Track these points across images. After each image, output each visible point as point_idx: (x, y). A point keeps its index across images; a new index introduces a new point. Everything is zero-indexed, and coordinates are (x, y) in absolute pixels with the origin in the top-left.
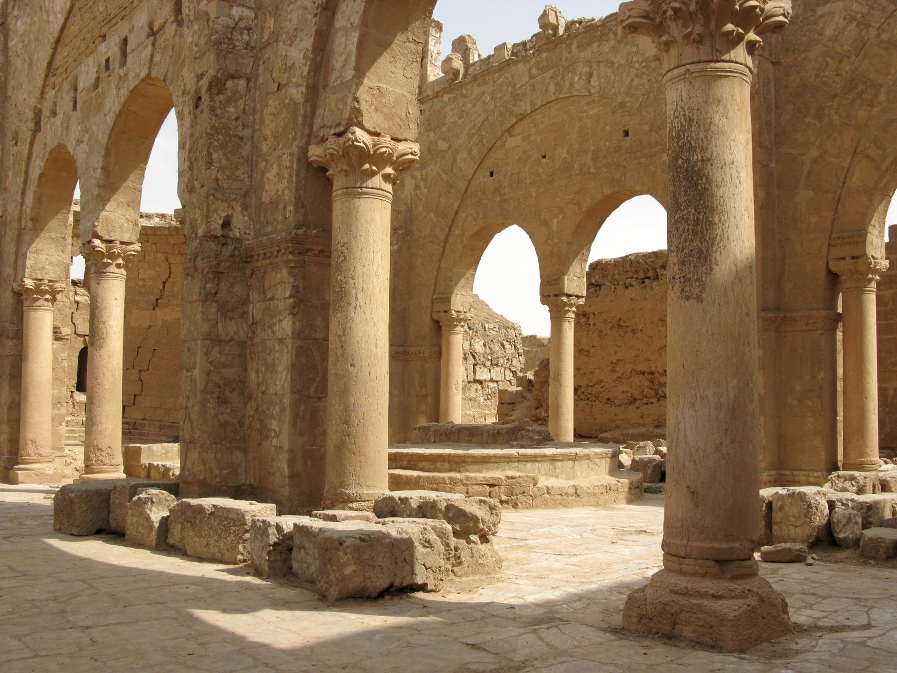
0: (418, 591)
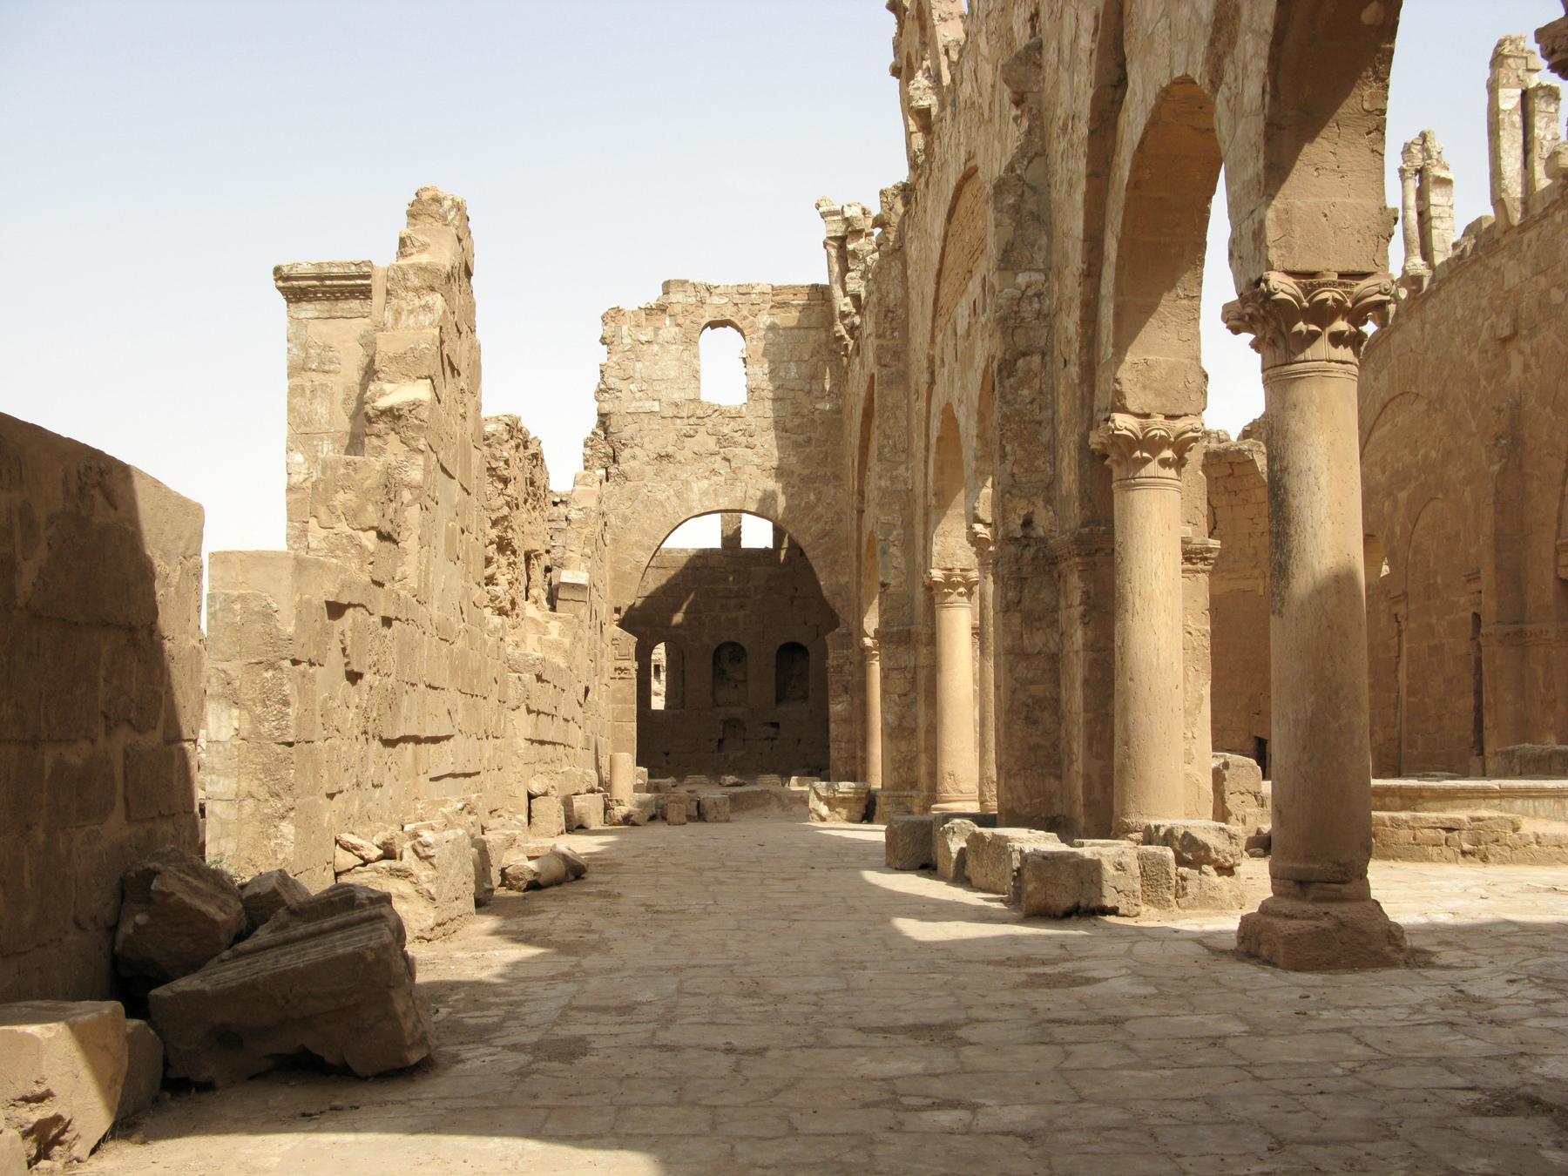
0: (1110, 914)
